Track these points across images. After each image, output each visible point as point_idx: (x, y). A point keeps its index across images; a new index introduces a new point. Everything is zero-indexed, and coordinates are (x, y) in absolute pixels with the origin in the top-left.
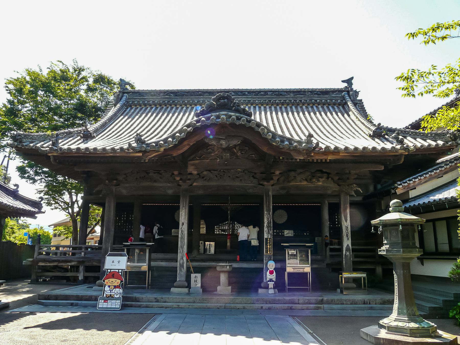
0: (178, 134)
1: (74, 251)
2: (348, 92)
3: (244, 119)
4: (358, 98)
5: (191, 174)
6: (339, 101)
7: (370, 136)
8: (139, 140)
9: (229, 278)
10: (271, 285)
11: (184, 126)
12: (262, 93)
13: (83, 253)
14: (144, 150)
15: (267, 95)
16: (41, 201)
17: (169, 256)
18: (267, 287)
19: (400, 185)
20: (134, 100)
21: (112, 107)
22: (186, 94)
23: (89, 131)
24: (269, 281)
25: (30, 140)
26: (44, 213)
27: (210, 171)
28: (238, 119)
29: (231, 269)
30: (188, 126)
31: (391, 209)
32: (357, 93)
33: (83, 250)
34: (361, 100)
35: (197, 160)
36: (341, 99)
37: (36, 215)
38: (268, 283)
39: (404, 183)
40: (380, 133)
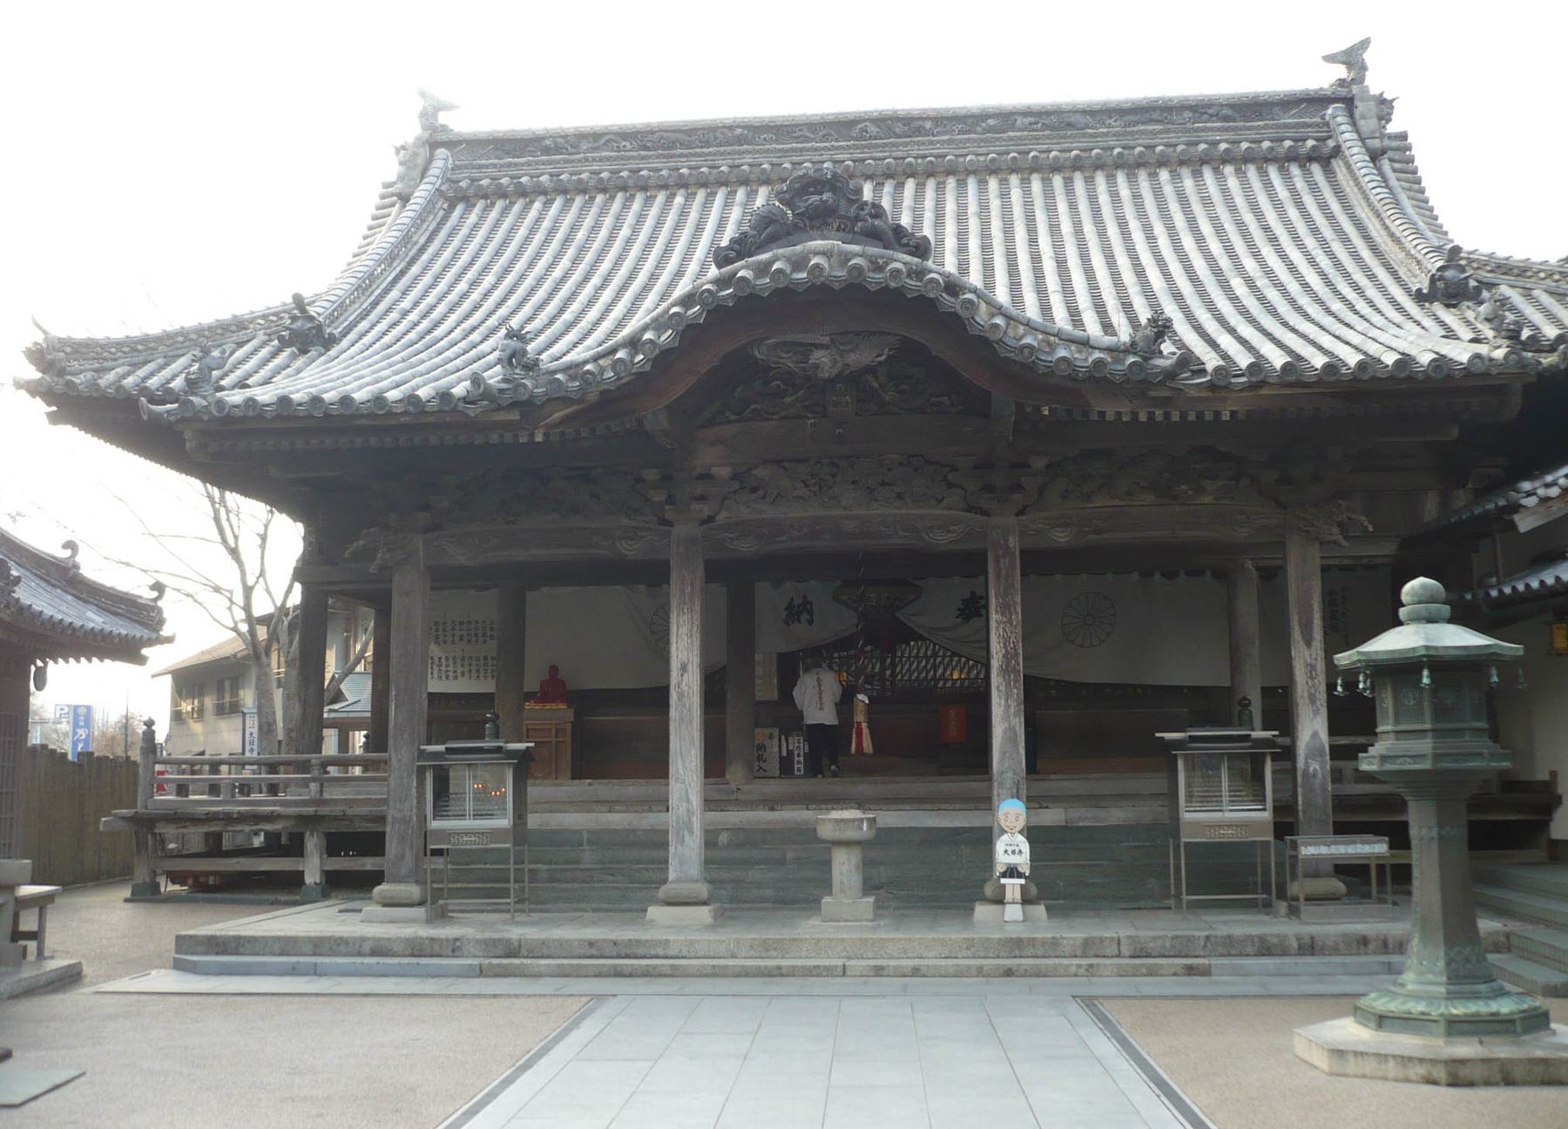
0: (648, 336)
2: (1349, 102)
3: (898, 271)
5: (706, 476)
7: (1420, 298)
9: (867, 864)
10: (1013, 886)
11: (673, 305)
12: (991, 122)
14: (525, 398)
15: (1013, 128)
16: (156, 600)
17: (633, 788)
18: (1000, 901)
19: (1529, 494)
21: (393, 205)
23: (312, 318)
24: (1004, 875)
26: (170, 640)
27: (778, 462)
29: (872, 834)
30: (687, 301)
31: (1402, 612)
32: (1384, 107)
33: (316, 773)
34: (1403, 136)
35: (730, 422)
36: (1317, 136)
37: (145, 651)
38: (1003, 881)
39: (1547, 486)
40: (1455, 283)
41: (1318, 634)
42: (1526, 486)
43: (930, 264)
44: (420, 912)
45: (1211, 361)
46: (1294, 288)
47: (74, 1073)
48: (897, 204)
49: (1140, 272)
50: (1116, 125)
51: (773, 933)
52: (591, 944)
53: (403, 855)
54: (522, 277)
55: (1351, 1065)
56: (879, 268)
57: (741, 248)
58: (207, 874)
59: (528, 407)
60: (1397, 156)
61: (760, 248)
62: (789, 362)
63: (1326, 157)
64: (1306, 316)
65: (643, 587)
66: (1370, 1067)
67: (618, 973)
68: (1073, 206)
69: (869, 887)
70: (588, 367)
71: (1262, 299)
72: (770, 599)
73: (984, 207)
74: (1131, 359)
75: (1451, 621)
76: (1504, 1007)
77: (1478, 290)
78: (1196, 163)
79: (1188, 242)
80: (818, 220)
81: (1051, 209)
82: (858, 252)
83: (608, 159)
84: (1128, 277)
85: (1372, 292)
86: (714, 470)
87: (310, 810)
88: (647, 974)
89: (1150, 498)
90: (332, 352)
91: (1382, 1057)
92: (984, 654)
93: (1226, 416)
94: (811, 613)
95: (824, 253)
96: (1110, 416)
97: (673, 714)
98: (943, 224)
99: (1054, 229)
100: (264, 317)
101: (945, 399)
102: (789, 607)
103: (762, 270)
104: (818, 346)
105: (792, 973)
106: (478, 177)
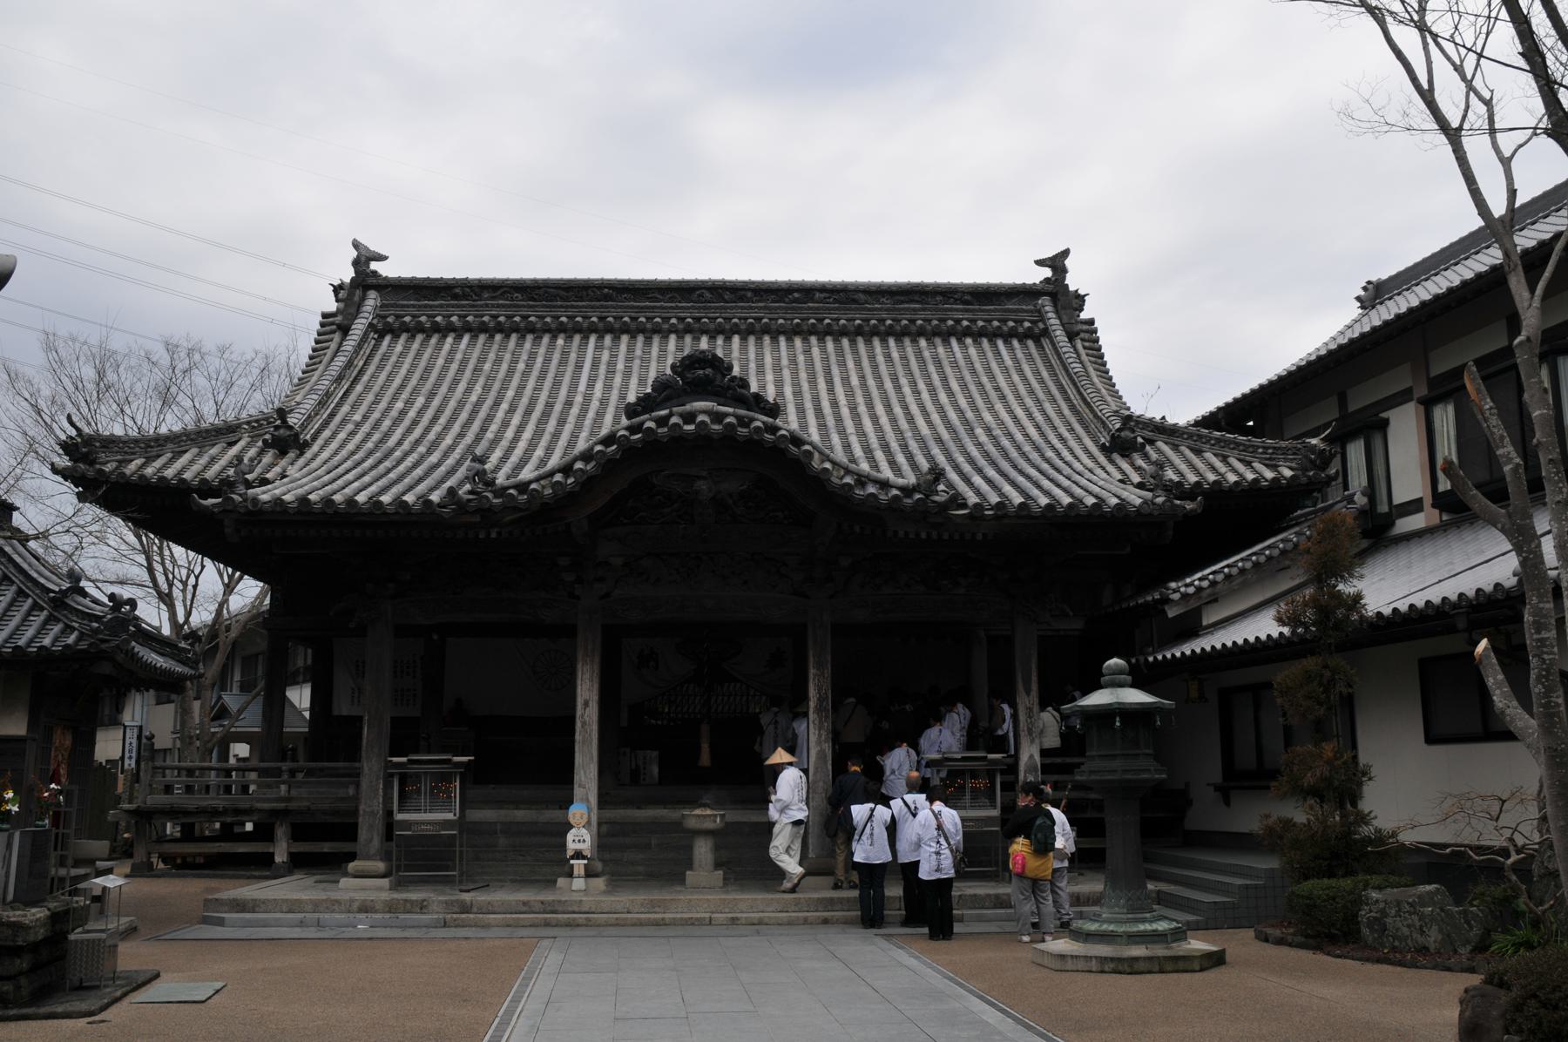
4: (1084, 316)
6: (1027, 324)
8: (481, 477)
9: (717, 848)
13: (283, 787)
19: (1175, 591)
21: (333, 332)
22: (562, 293)
28: (744, 422)
32: (1079, 300)
33: (285, 777)
34: (1091, 322)
36: (1038, 317)
39: (1187, 586)
41: (1035, 687)
42: (1173, 585)
43: (779, 422)
44: (385, 882)
45: (973, 499)
46: (1019, 437)
48: (729, 352)
49: (910, 419)
50: (887, 302)
51: (657, 895)
52: (524, 903)
53: (371, 840)
54: (445, 400)
55: (1070, 965)
57: (645, 404)
58: (194, 856)
59: (487, 513)
60: (1086, 336)
61: (659, 407)
63: (1039, 335)
64: (1028, 460)
66: (1081, 965)
67: (547, 924)
68: (858, 363)
69: (718, 865)
70: (533, 486)
71: (997, 445)
73: (793, 361)
74: (918, 496)
75: (1132, 686)
76: (1162, 926)
77: (1143, 446)
78: (946, 335)
79: (943, 397)
80: (701, 389)
81: (842, 364)
83: (504, 306)
84: (903, 424)
85: (1072, 443)
87: (282, 805)
88: (569, 925)
90: (308, 454)
91: (1087, 958)
93: (979, 537)
96: (901, 534)
97: (578, 737)
98: (763, 373)
99: (846, 381)
100: (248, 423)
103: (662, 422)
104: (699, 478)
105: (673, 923)
106: (386, 308)
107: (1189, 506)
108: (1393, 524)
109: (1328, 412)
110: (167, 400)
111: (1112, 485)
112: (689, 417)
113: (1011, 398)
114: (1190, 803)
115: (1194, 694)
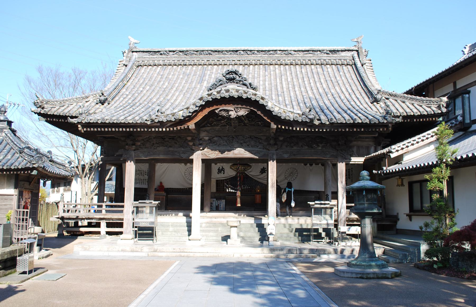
1: (100, 209)
20: (143, 60)
22: (195, 52)
25: (51, 106)
35: (208, 126)
43: (257, 93)
47: (65, 274)
56: (246, 93)
57: (214, 86)
62: (224, 114)
65: (183, 164)
72: (215, 168)
80: (231, 80)
82: (242, 89)
86: (205, 138)
89: (306, 147)
91: (352, 273)
92: (266, 182)
94: (224, 171)
95: (233, 89)
101: (260, 123)
102: (219, 170)
107: (397, 120)
108: (471, 127)
109: (449, 88)
110: (75, 88)
111: (375, 112)
112: (227, 91)
113: (341, 85)
114: (399, 220)
115: (400, 183)
